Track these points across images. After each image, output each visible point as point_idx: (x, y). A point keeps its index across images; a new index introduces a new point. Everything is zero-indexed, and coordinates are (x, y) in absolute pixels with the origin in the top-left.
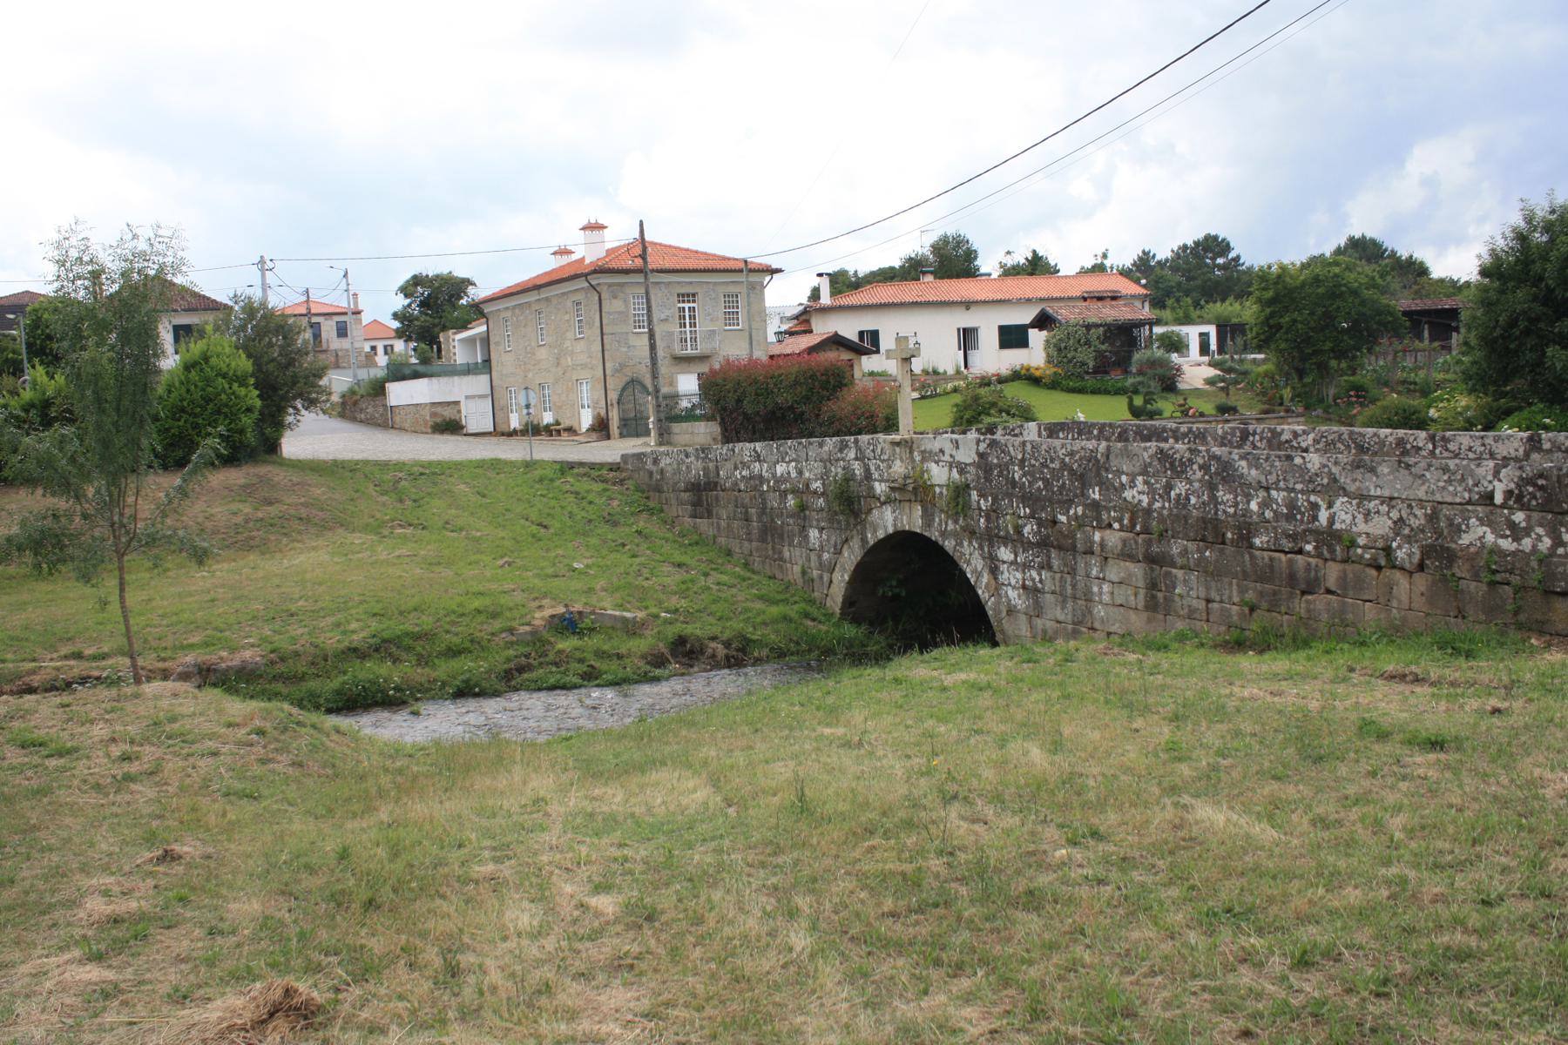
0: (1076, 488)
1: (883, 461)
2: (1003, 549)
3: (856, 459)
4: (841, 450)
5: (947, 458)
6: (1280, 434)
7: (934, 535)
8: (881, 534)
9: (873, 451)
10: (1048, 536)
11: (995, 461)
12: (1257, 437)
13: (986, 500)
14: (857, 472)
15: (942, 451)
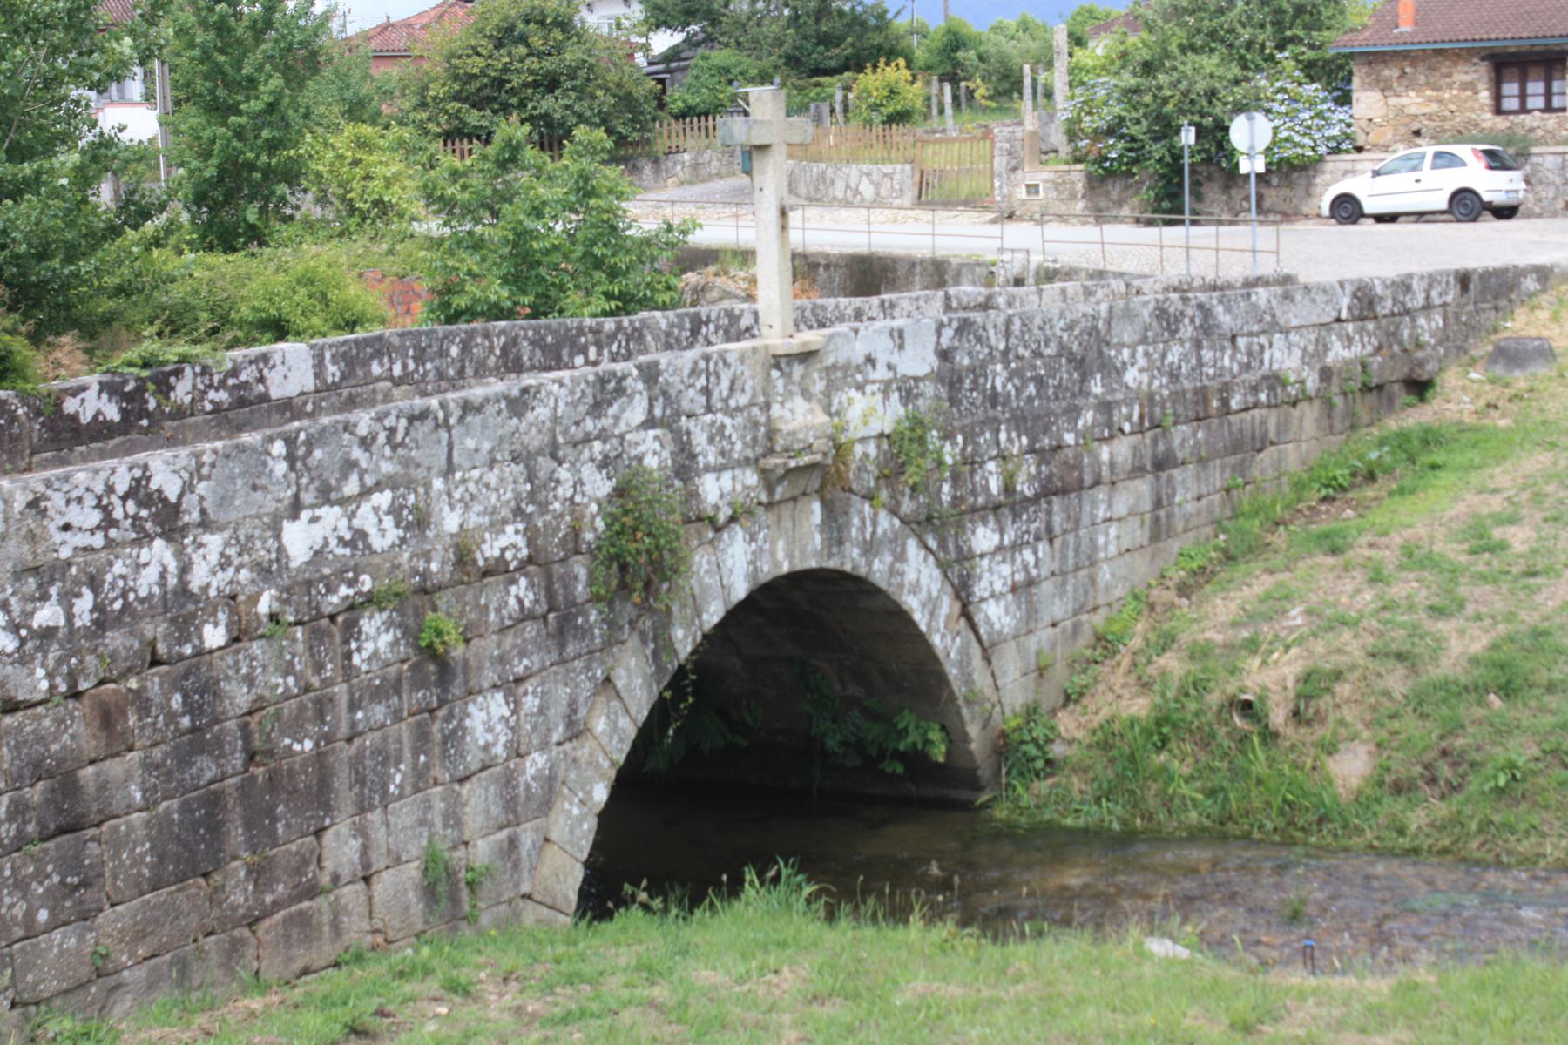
0: (1074, 383)
1: (731, 413)
2: (980, 530)
3: (649, 423)
4: (597, 409)
5: (881, 373)
6: (739, 318)
7: (851, 559)
8: (713, 614)
9: (706, 391)
10: (1050, 477)
11: (966, 361)
12: (712, 327)
13: (954, 444)
14: (651, 462)
15: (870, 360)
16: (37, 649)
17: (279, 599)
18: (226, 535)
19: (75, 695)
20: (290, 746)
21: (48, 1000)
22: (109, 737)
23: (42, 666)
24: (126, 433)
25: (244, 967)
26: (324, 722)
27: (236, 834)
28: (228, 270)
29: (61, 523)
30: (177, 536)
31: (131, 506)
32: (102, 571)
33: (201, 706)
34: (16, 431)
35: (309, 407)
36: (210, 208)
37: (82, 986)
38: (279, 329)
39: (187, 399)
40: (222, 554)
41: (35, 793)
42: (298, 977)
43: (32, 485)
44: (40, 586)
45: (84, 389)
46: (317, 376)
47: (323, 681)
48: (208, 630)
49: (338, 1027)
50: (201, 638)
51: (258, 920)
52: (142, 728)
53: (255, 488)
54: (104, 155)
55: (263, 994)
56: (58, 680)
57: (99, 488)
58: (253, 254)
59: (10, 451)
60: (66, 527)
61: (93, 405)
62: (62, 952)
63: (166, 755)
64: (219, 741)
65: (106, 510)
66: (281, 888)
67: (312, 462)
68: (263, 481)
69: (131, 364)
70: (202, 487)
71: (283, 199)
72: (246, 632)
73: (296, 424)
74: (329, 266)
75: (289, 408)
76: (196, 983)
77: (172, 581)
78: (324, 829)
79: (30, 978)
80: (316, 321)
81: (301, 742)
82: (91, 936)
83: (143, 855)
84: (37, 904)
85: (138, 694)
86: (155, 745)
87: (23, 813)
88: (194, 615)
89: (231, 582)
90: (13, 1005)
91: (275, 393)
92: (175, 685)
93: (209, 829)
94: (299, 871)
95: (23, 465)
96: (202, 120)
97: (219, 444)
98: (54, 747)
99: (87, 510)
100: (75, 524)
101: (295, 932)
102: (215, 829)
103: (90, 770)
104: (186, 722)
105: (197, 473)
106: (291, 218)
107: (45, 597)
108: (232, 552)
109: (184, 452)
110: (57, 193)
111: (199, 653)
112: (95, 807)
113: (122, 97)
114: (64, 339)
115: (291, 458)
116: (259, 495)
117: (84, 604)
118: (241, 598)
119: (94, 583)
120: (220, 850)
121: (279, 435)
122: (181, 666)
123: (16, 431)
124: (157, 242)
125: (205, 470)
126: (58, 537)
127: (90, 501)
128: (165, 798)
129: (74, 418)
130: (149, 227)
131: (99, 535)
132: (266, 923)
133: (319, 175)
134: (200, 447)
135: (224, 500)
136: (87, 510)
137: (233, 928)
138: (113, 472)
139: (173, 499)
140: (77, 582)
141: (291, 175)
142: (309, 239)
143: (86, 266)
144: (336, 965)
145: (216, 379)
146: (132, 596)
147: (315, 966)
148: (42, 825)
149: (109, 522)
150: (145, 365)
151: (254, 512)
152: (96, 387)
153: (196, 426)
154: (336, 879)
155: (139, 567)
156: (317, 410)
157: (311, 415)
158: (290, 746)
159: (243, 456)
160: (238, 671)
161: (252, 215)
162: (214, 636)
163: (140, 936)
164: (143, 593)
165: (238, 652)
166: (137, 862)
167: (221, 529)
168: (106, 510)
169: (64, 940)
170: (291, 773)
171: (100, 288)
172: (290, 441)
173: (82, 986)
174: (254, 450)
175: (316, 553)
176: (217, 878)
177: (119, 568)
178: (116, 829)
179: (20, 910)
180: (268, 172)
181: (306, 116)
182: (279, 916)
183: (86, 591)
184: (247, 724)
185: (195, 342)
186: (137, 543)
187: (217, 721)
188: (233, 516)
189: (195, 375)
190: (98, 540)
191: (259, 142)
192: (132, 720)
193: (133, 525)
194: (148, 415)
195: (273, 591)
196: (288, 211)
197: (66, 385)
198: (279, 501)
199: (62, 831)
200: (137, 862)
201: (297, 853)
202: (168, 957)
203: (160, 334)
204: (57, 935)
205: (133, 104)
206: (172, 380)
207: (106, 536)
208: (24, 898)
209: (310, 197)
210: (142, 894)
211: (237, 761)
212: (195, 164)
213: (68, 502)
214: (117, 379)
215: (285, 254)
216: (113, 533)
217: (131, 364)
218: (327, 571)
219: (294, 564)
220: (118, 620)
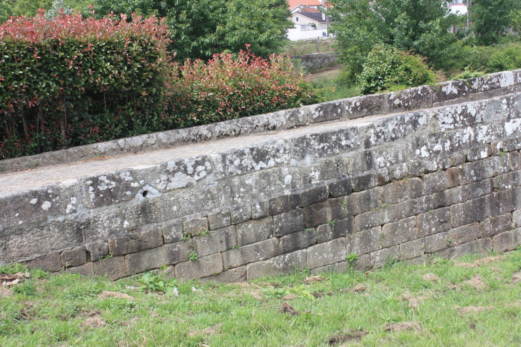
16: (434, 156)
17: (503, 145)
18: (488, 126)
19: (445, 170)
20: (504, 187)
21: (434, 252)
22: (453, 181)
23: (436, 161)
24: (459, 97)
25: (489, 248)
26: (515, 180)
27: (488, 211)
28: (486, 51)
29: (442, 122)
30: (474, 126)
31: (462, 117)
32: (453, 135)
33: (479, 174)
34: (429, 96)
35: (512, 90)
36: (482, 33)
37: (443, 249)
38: (501, 68)
39: (476, 88)
40: (487, 131)
41: (433, 196)
42: (504, 252)
43: (435, 111)
44: (436, 139)
45: (448, 85)
46: (515, 81)
47: (515, 168)
48: (482, 152)
49: (517, 267)
50: (480, 155)
51: (493, 235)
52: (462, 180)
53: (497, 113)
54: (453, 19)
55: (494, 256)
56: (440, 165)
57: (453, 112)
58: (494, 46)
59: (427, 102)
60: (444, 123)
61: (450, 88)
62: (438, 240)
63: (469, 187)
64: (484, 184)
65: (455, 118)
66: (500, 227)
67: (514, 105)
68: (500, 111)
69: (461, 78)
70: (482, 112)
71: (503, 31)
72: (493, 154)
73: (510, 94)
74: (516, 49)
75: (506, 90)
76: (475, 251)
77: (472, 139)
78: (513, 211)
79: (429, 246)
80: (512, 65)
81: (508, 186)
82: (446, 236)
83: (461, 215)
84: (432, 226)
85: (462, 170)
86: (466, 184)
87: (429, 201)
88: (478, 148)
89: (489, 139)
90: (425, 253)
91: (502, 86)
92: (472, 168)
93: (480, 209)
94: (505, 222)
95: (430, 106)
96: (481, 8)
97: (487, 100)
98: (438, 184)
99: (449, 118)
100: (446, 122)
101: (504, 240)
102: (482, 209)
103: (448, 190)
104: (475, 178)
105: (481, 108)
106: (505, 35)
107: (437, 142)
108: (490, 131)
109: (477, 102)
110: (436, 31)
111: (479, 159)
112: (449, 201)
113: (456, 3)
114: (439, 71)
115: (508, 104)
116: (498, 115)
117: (448, 144)
118: (492, 144)
119: (451, 139)
120: (483, 215)
121: (505, 98)
122: (474, 163)
123: (429, 96)
124: (466, 44)
125: (483, 107)
126: (441, 125)
127: (450, 116)
128: (468, 199)
129: (445, 93)
130: (464, 39)
131: (453, 125)
132: (496, 236)
133: (514, 22)
134: (481, 101)
135: (488, 116)
136: (449, 118)
137: (486, 237)
138: (457, 108)
139: (473, 115)
140: (446, 138)
141: (506, 23)
142: (510, 41)
143: (445, 51)
144: (515, 249)
145: (485, 82)
146: (461, 143)
147: (509, 249)
148: (434, 205)
149: (455, 122)
150: (465, 78)
151: (497, 119)
152: (451, 84)
153: (479, 95)
154: (516, 225)
155: (463, 134)
156: (514, 90)
157: (512, 92)
158: (504, 187)
159: (494, 104)
160: (490, 165)
161: (494, 35)
162: (484, 154)
163: (460, 237)
164: (464, 142)
165: (490, 159)
166: (460, 216)
167: (487, 124)
168: (455, 118)
169: (439, 236)
170: (504, 194)
171: (450, 56)
172: (508, 99)
173: (443, 249)
174: (497, 102)
175: (514, 132)
176: (482, 223)
177: (457, 135)
178: (454, 207)
179: (427, 227)
180: (499, 22)
181: (511, 5)
182: (499, 235)
183: (448, 141)
184: (492, 180)
185: (479, 71)
186: (463, 128)
187: (484, 179)
188: (490, 120)
189: (479, 80)
190: (452, 127)
191: (497, 13)
192: (460, 177)
193: (462, 122)
194: (465, 92)
195: (501, 142)
196: (504, 33)
197: (443, 83)
198: (504, 116)
199: (440, 207)
200: (460, 216)
201: (506, 217)
202: (467, 243)
203: (469, 69)
204: (437, 235)
205: (460, 4)
206: (473, 82)
207: (454, 126)
208: (429, 224)
209: (511, 29)
210: (461, 225)
211: (489, 190)
212: (478, 21)
213: (444, 116)
214: (457, 82)
215: (504, 46)
216: (456, 125)
217: (461, 78)
218: (517, 137)
219: (508, 135)
220: (457, 149)
